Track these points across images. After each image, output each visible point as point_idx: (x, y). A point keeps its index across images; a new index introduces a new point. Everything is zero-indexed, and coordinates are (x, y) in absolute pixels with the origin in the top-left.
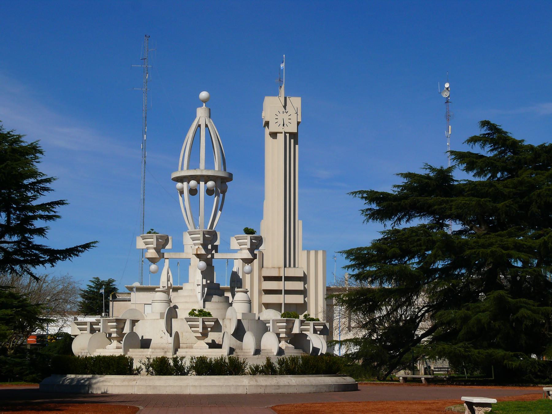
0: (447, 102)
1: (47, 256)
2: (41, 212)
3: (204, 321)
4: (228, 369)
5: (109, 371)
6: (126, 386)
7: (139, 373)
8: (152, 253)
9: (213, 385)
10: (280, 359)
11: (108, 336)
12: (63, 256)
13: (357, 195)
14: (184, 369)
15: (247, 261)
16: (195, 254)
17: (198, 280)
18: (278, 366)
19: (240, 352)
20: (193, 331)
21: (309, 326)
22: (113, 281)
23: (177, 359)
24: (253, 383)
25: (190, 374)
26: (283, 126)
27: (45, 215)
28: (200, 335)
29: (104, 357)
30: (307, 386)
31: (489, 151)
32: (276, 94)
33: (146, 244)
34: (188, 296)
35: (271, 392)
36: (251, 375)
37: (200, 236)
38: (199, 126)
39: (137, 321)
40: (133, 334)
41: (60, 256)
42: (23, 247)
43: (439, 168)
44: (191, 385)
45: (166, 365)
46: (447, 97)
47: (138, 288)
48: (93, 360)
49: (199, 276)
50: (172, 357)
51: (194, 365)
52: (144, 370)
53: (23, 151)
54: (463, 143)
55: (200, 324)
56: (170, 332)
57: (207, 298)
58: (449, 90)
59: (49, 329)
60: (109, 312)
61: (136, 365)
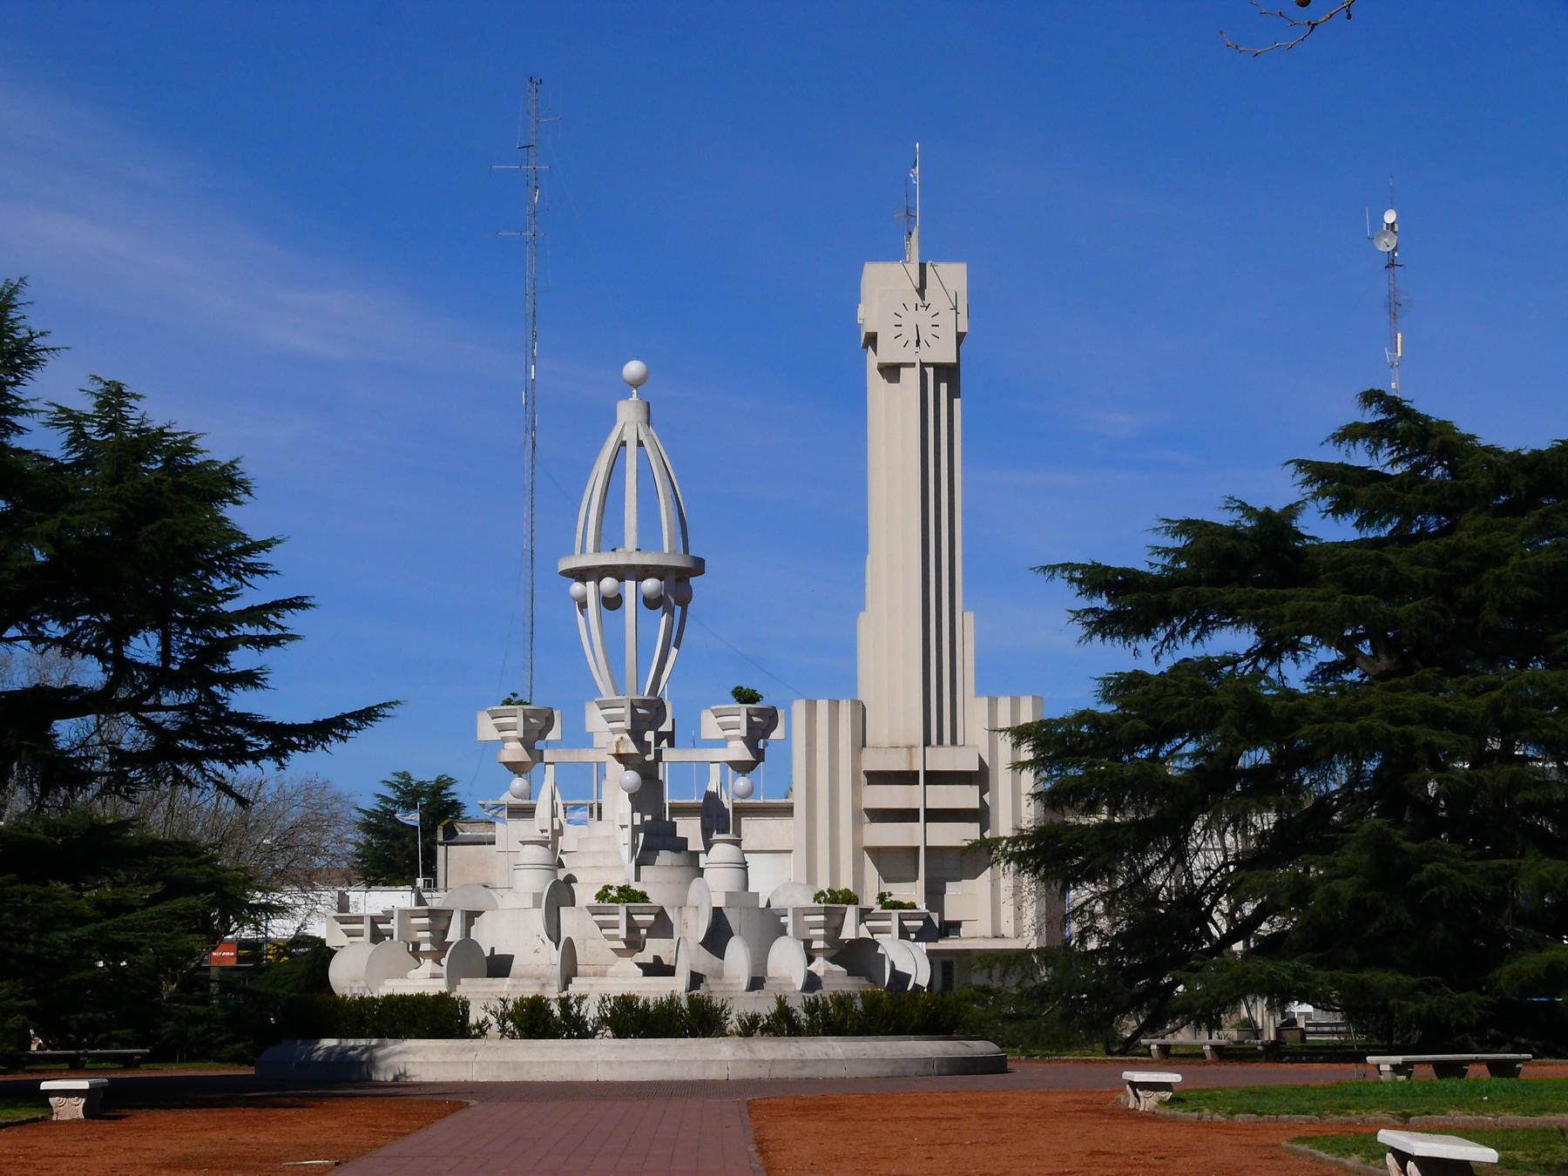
0: (1391, 265)
1: (267, 740)
2: (246, 630)
3: (631, 912)
4: (688, 1023)
5: (415, 1030)
6: (453, 1063)
7: (483, 1033)
8: (514, 751)
9: (649, 1059)
10: (810, 1000)
11: (411, 950)
12: (306, 739)
13: (1056, 574)
14: (585, 1024)
15: (742, 768)
16: (613, 755)
17: (622, 816)
18: (804, 1016)
19: (717, 984)
20: (606, 936)
21: (890, 920)
22: (451, 781)
23: (568, 1000)
24: (743, 1054)
25: (600, 1036)
26: (918, 345)
27: (258, 636)
28: (622, 945)
29: (403, 998)
30: (870, 1061)
31: (1388, 464)
32: (898, 255)
33: (501, 728)
34: (600, 852)
35: (785, 1076)
36: (740, 1036)
37: (625, 711)
38: (624, 444)
39: (479, 913)
40: (467, 944)
41: (300, 741)
42: (204, 718)
43: (1260, 507)
44: (599, 1059)
45: (544, 1016)
46: (1389, 249)
47: (513, 807)
48: (377, 1005)
49: (625, 805)
50: (557, 996)
51: (609, 1015)
52: (495, 1027)
53: (200, 487)
54: (1323, 443)
55: (622, 919)
56: (556, 941)
57: (644, 858)
58: (1396, 229)
59: (269, 924)
60: (434, 874)
61: (475, 1016)
